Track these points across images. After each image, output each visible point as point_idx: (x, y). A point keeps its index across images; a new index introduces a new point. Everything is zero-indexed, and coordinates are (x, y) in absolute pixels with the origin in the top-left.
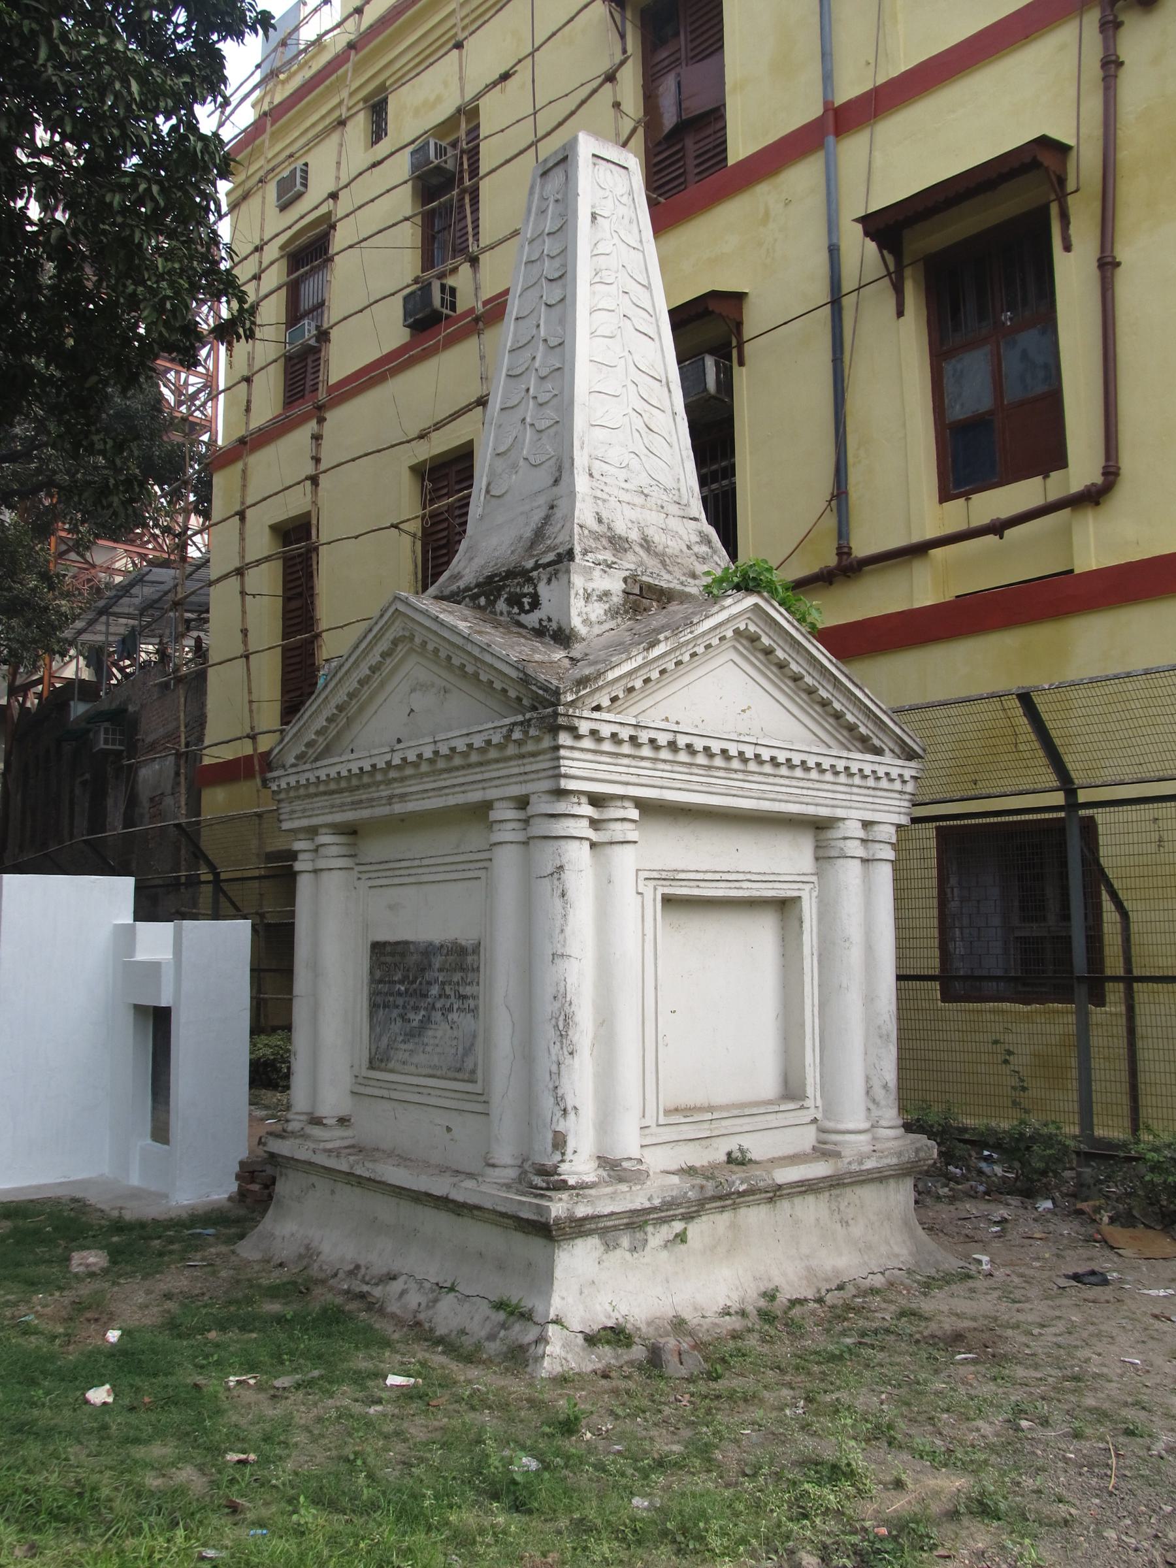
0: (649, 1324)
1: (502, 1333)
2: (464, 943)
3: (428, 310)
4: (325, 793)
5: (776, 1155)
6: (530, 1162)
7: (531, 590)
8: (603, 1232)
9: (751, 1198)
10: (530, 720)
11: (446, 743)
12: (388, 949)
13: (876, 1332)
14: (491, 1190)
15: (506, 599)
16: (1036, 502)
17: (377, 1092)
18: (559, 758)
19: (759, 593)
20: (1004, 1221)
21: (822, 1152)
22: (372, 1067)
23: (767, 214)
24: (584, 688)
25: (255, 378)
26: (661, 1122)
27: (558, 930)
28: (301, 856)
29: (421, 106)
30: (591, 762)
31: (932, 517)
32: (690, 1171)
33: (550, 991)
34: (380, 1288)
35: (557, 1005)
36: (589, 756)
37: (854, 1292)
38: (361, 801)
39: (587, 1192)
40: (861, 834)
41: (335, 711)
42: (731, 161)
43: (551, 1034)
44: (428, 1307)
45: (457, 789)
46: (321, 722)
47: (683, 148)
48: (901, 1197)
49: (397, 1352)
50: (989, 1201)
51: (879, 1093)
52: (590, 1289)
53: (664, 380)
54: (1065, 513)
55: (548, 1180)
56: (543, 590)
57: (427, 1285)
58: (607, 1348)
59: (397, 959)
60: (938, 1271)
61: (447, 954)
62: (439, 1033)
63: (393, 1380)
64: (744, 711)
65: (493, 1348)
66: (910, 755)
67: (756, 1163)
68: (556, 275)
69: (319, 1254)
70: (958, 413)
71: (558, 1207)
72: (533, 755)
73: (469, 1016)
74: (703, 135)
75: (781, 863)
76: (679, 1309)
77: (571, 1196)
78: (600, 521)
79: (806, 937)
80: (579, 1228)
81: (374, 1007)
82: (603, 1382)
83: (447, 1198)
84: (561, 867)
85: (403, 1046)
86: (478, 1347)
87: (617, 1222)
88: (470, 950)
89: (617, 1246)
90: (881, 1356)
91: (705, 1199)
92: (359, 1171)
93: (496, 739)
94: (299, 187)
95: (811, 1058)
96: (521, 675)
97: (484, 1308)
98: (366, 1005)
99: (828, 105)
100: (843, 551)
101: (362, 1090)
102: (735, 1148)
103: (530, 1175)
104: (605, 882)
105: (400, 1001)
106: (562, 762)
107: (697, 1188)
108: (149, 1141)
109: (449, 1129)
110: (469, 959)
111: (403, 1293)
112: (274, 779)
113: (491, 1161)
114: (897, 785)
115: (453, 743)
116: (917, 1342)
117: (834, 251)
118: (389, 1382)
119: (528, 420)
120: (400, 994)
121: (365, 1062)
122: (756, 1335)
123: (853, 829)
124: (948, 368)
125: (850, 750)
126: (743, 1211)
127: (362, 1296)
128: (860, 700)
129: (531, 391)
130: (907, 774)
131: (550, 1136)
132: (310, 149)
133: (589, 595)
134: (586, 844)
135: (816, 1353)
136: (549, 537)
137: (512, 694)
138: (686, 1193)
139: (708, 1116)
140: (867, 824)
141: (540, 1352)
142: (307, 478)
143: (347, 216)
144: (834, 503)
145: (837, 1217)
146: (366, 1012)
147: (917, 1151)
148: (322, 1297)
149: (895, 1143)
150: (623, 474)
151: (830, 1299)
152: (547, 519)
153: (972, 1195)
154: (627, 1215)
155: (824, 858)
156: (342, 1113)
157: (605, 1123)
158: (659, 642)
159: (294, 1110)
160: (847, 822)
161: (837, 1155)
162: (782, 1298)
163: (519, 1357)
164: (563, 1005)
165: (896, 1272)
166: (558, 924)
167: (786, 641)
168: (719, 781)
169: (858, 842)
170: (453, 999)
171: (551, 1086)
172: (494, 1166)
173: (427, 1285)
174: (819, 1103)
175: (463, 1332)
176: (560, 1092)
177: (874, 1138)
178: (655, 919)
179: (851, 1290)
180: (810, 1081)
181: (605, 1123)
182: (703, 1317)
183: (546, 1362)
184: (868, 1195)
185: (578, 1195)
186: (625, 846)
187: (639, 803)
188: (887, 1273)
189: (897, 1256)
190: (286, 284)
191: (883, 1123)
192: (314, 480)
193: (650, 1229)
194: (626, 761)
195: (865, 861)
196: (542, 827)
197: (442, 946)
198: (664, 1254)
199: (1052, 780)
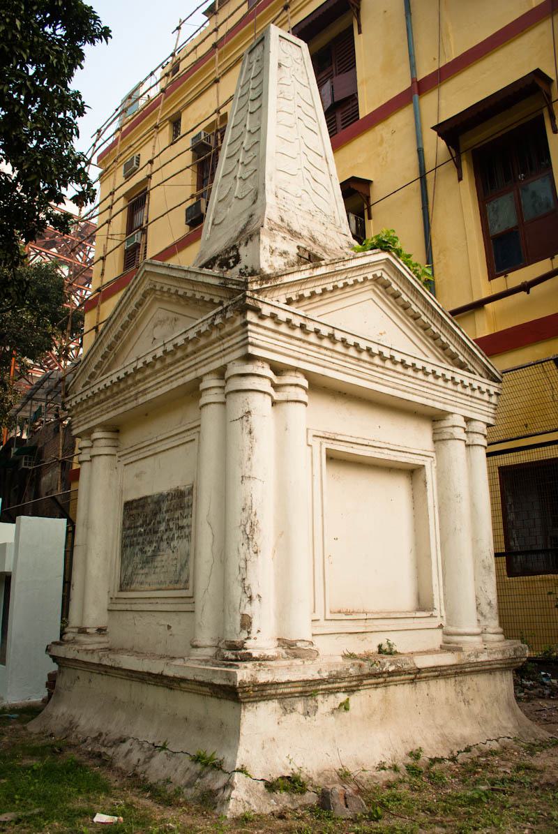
0: (319, 775)
1: (198, 781)
2: (182, 489)
5: (415, 651)
7: (235, 253)
8: (282, 697)
9: (398, 678)
10: (227, 307)
12: (135, 504)
13: (503, 781)
14: (195, 666)
17: (124, 607)
19: (389, 252)
21: (447, 648)
22: (121, 590)
23: (382, 141)
24: (266, 283)
25: (108, 257)
26: (327, 618)
27: (246, 459)
29: (197, 117)
30: (272, 338)
31: (485, 288)
32: (351, 656)
33: (239, 505)
34: (113, 749)
35: (245, 515)
37: (478, 754)
39: (268, 663)
40: (464, 424)
42: (361, 117)
43: (240, 537)
44: (145, 762)
45: (179, 375)
47: (335, 117)
48: (504, 686)
49: (112, 796)
51: (486, 609)
52: (271, 745)
53: (324, 157)
55: (236, 653)
57: (146, 745)
58: (284, 793)
59: (140, 510)
60: (535, 740)
61: (172, 499)
62: (166, 558)
63: (101, 818)
65: (189, 793)
67: (400, 654)
68: (256, 96)
70: (496, 230)
71: (244, 674)
72: (229, 334)
73: (185, 540)
74: (346, 109)
75: (410, 440)
76: (344, 764)
77: (254, 665)
78: (282, 220)
79: (429, 494)
80: (262, 692)
81: (124, 547)
82: (279, 822)
83: (161, 675)
84: (249, 412)
85: (141, 572)
86: (178, 793)
87: (293, 690)
88: (187, 493)
89: (293, 710)
90: (512, 800)
91: (363, 675)
94: (135, 165)
97: (186, 761)
99: (414, 80)
101: (115, 607)
102: (384, 642)
103: (223, 651)
104: (283, 429)
105: (140, 540)
107: (356, 666)
109: (169, 627)
110: (186, 499)
111: (130, 751)
113: (195, 643)
116: (536, 788)
117: (420, 152)
118: (95, 820)
120: (141, 534)
121: (117, 587)
122: (407, 785)
124: (489, 207)
126: (392, 688)
127: (99, 755)
130: (492, 390)
131: (239, 618)
132: (141, 147)
133: (273, 251)
134: (268, 400)
135: (457, 798)
138: (348, 669)
139: (364, 616)
140: (468, 420)
141: (227, 796)
143: (158, 170)
145: (461, 697)
146: (119, 551)
147: (515, 650)
148: (71, 755)
149: (500, 644)
150: (298, 201)
151: (460, 758)
153: (542, 697)
154: (301, 684)
155: (440, 440)
157: (283, 611)
158: (321, 266)
159: (70, 626)
160: (454, 415)
161: (460, 650)
162: (425, 757)
163: (210, 801)
164: (250, 515)
165: (506, 739)
166: (247, 453)
167: (408, 289)
168: (365, 370)
169: (462, 430)
171: (240, 578)
172: (196, 647)
173: (146, 745)
174: (443, 614)
175: (168, 781)
176: (247, 583)
178: (321, 465)
179: (475, 753)
180: (436, 597)
181: (283, 611)
182: (364, 770)
183: (232, 804)
184: (481, 681)
185: (260, 665)
186: (298, 404)
187: (306, 374)
188: (500, 740)
189: (505, 728)
190: (127, 206)
191: (489, 630)
193: (320, 698)
195: (468, 446)
197: (168, 494)
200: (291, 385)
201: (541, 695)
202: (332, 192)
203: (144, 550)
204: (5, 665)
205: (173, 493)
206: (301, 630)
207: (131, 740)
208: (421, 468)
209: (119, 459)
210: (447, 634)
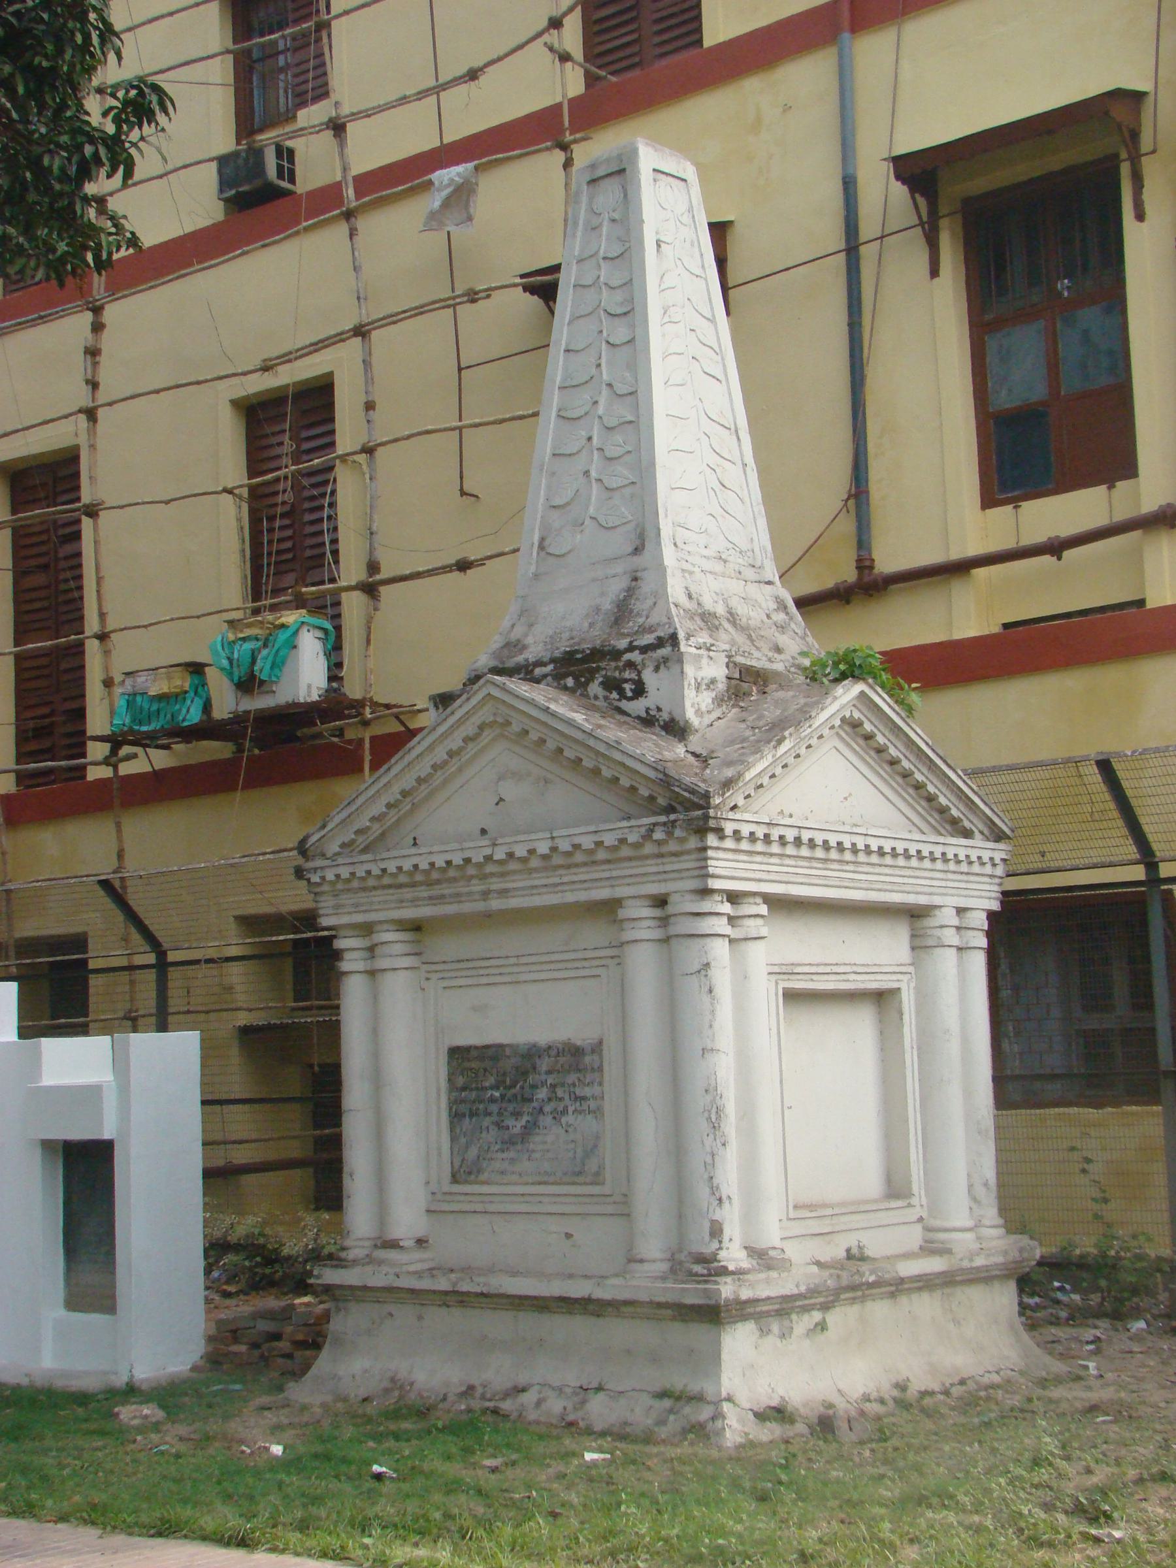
2: (579, 1043)
3: (258, 183)
4: (390, 886)
6: (686, 1253)
7: (634, 676)
8: (758, 1317)
10: (675, 821)
11: (567, 839)
12: (474, 1053)
14: (648, 1281)
15: (602, 683)
16: (1100, 520)
18: (706, 859)
19: (864, 679)
20: (1097, 1340)
21: (929, 1249)
22: (455, 1179)
26: (791, 1215)
27: (707, 1025)
28: (347, 956)
31: (977, 529)
35: (709, 1098)
36: (730, 856)
38: (443, 896)
40: (955, 921)
41: (399, 797)
42: (708, 42)
43: (704, 1126)
46: (378, 808)
50: (1073, 1326)
52: (755, 1372)
54: (1136, 535)
55: (710, 1267)
56: (648, 676)
57: (568, 1390)
64: (846, 798)
66: (998, 836)
68: (619, 311)
69: (412, 1384)
70: (1004, 400)
71: (727, 1289)
73: (589, 1117)
75: (877, 954)
77: (734, 1280)
78: (690, 597)
79: (906, 1030)
80: (743, 1310)
81: (456, 1117)
84: (708, 965)
85: (500, 1155)
87: (771, 1307)
92: (465, 1287)
93: (633, 838)
95: (915, 1155)
96: (661, 776)
98: (444, 1115)
100: (864, 564)
102: (854, 1244)
104: (742, 977)
105: (494, 1108)
106: (710, 862)
108: (62, 1312)
109: (568, 1236)
110: (587, 1059)
112: (315, 870)
114: (988, 869)
115: (577, 840)
117: (849, 185)
119: (593, 474)
120: (492, 1100)
123: (948, 916)
124: (992, 344)
125: (941, 835)
126: (869, 1304)
128: (953, 782)
129: (595, 440)
136: (639, 615)
137: (644, 792)
140: (960, 911)
142: (80, 411)
144: (851, 502)
147: (1021, 1250)
152: (630, 592)
153: (1055, 1322)
155: (921, 948)
156: (420, 1234)
157: (750, 1216)
158: (785, 738)
160: (943, 910)
161: (949, 1252)
163: (700, 1431)
164: (715, 1098)
167: (886, 726)
170: (567, 1101)
171: (706, 1176)
172: (641, 1261)
173: (568, 1390)
174: (924, 1201)
176: (715, 1181)
177: (978, 1238)
180: (915, 1178)
183: (728, 1433)
184: (975, 1295)
187: (768, 899)
192: (91, 414)
193: (794, 1317)
194: (758, 858)
195: (960, 949)
196: (684, 926)
198: (807, 1343)
199: (1130, 850)
200: (750, 916)
201: (1053, 1319)
202: (747, 500)
203: (504, 1124)
204: (111, 1309)
205: (561, 1047)
206: (772, 1234)
207: (537, 1387)
208: (895, 992)
209: (428, 975)
210: (928, 1229)
